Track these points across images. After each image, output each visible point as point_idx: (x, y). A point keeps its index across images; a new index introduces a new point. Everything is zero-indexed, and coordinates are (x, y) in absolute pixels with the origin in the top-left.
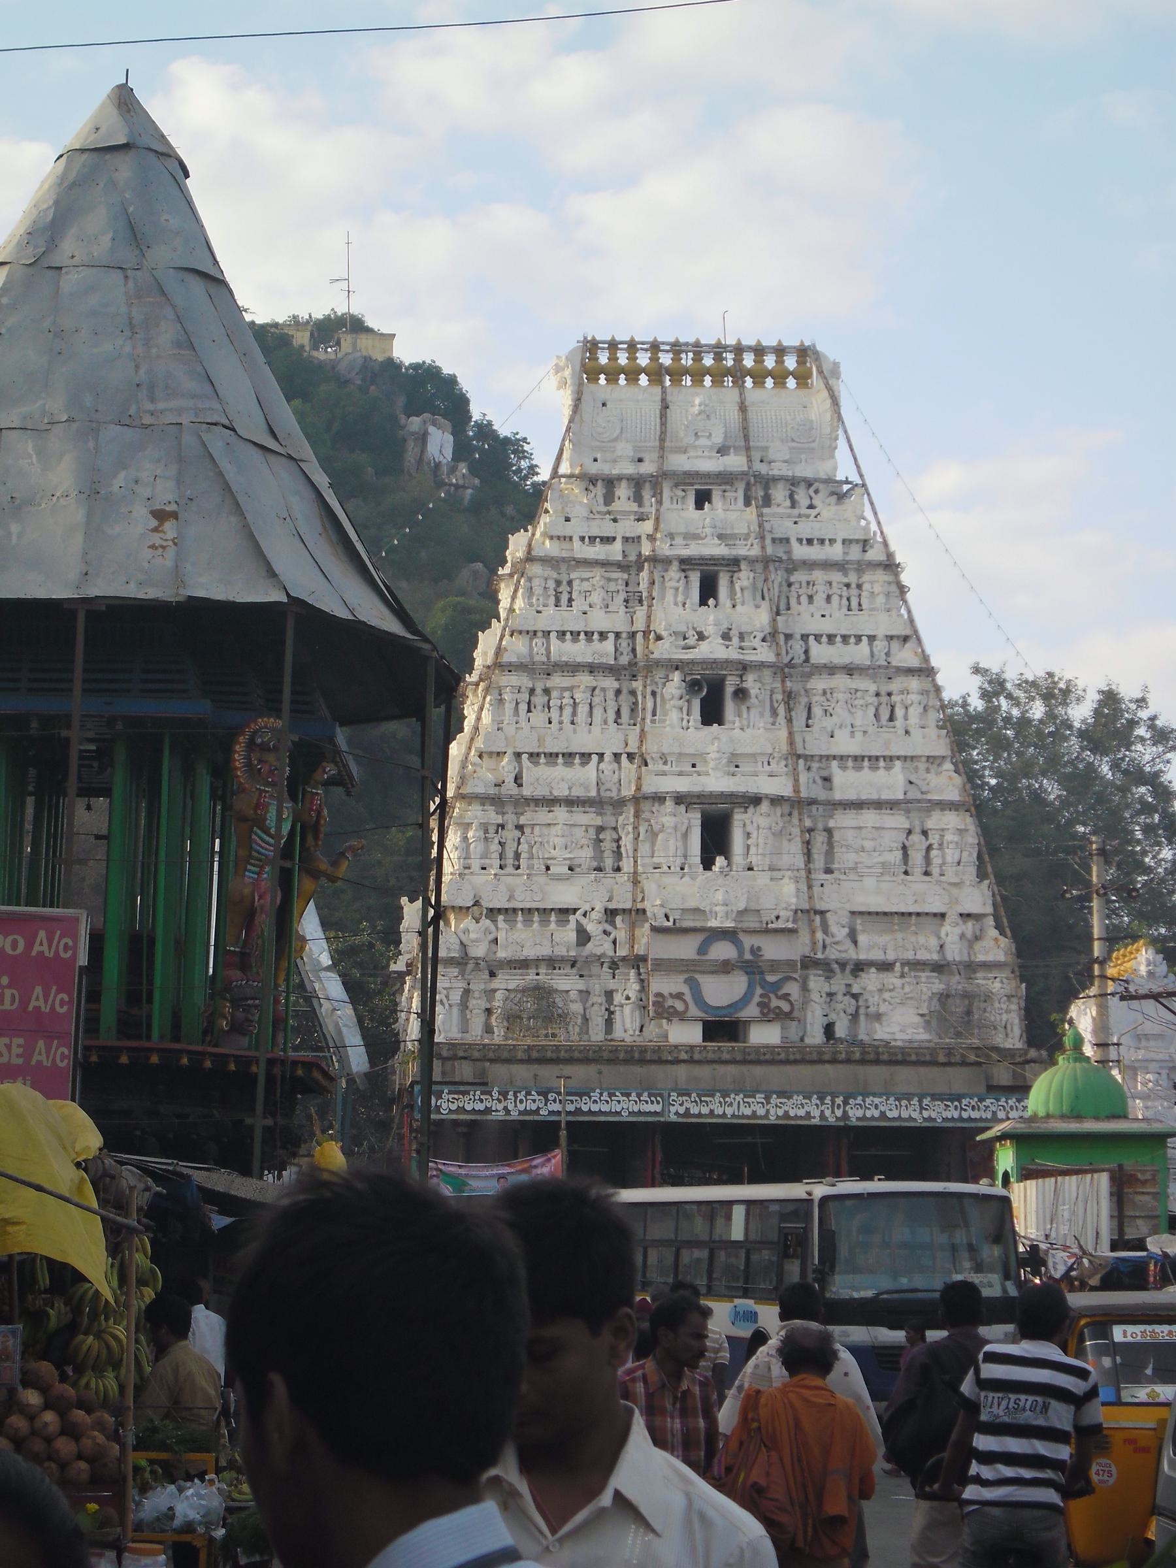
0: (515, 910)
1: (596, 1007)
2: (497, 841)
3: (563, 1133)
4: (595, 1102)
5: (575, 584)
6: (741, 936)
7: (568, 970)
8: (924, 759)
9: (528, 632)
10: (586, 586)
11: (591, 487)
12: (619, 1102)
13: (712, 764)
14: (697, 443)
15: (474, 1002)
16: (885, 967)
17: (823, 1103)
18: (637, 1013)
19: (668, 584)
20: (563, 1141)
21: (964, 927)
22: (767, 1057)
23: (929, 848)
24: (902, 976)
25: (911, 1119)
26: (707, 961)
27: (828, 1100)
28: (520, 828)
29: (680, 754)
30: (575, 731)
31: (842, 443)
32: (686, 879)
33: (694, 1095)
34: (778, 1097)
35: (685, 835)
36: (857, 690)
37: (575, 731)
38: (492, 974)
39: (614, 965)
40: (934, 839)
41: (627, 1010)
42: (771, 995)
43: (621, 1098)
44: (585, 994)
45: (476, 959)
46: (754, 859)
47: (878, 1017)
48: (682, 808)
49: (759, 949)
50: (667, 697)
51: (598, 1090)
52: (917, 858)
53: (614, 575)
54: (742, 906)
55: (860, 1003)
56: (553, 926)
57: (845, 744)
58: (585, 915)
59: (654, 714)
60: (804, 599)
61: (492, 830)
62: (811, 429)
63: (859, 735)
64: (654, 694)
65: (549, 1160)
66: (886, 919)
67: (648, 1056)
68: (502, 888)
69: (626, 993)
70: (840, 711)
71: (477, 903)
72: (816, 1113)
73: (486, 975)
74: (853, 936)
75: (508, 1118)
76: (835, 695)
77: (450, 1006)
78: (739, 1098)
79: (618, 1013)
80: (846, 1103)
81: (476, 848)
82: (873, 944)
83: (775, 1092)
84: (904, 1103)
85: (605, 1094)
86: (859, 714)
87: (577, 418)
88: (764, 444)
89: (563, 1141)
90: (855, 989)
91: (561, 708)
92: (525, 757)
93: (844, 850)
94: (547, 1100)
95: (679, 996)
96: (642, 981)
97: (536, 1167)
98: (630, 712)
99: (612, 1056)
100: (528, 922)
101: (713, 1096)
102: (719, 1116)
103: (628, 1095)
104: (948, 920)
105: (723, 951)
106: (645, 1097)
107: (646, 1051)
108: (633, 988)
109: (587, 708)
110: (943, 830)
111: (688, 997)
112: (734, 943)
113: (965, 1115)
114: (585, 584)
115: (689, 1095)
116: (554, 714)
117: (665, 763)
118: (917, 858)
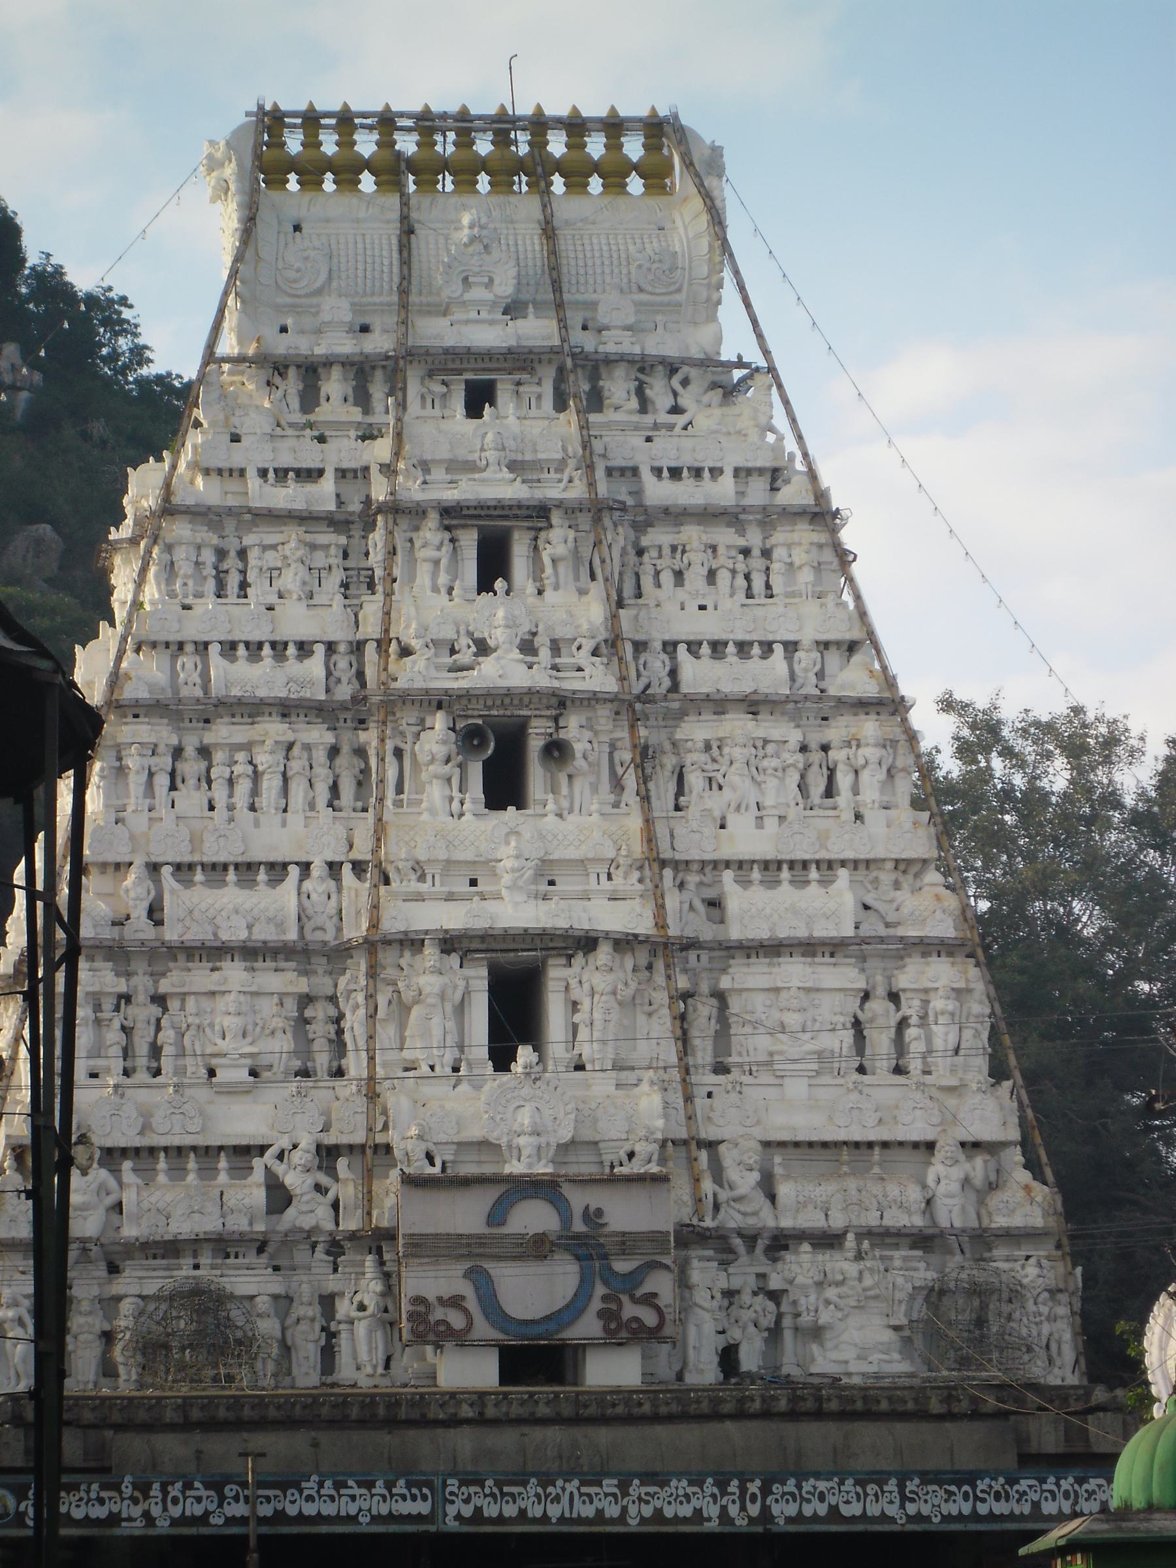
0: (152, 1151)
1: (303, 1327)
2: (116, 1024)
4: (310, 1498)
5: (253, 555)
6: (567, 1190)
7: (252, 1258)
8: (890, 865)
9: (167, 645)
11: (277, 380)
13: (506, 879)
14: (467, 296)
16: (827, 1240)
17: (724, 1493)
18: (379, 1334)
19: (421, 554)
22: (620, 1410)
23: (903, 1024)
24: (859, 1257)
25: (884, 1518)
27: (734, 1486)
28: (160, 1000)
29: (449, 862)
31: (729, 292)
33: (489, 1483)
35: (461, 1009)
37: (257, 824)
40: (911, 1007)
41: (361, 1328)
42: (625, 1299)
43: (357, 1491)
46: (586, 1050)
47: (817, 1333)
48: (454, 959)
49: (599, 1212)
50: (423, 758)
51: (315, 1478)
52: (881, 1042)
53: (322, 539)
55: (785, 1308)
56: (223, 1178)
57: (748, 840)
58: (280, 1156)
59: (400, 790)
60: (667, 578)
61: (108, 1004)
63: (771, 824)
64: (398, 753)
67: (403, 1413)
68: (129, 1110)
69: (357, 1298)
70: (738, 781)
75: (151, 1532)
76: (726, 750)
79: (344, 1335)
80: (766, 1491)
82: (804, 1200)
85: (328, 1483)
86: (771, 783)
90: (775, 1283)
91: (231, 782)
92: (166, 871)
93: (748, 1029)
94: (222, 1498)
95: (455, 1302)
96: (387, 1276)
98: (359, 786)
100: (178, 1173)
101: (524, 1484)
102: (535, 1521)
103: (370, 1485)
104: (939, 1154)
105: (533, 1217)
106: (400, 1488)
107: (398, 1403)
108: (371, 1288)
109: (277, 781)
111: (472, 1304)
113: (982, 1509)
114: (270, 554)
116: (219, 793)
117: (422, 878)
118: (881, 1042)
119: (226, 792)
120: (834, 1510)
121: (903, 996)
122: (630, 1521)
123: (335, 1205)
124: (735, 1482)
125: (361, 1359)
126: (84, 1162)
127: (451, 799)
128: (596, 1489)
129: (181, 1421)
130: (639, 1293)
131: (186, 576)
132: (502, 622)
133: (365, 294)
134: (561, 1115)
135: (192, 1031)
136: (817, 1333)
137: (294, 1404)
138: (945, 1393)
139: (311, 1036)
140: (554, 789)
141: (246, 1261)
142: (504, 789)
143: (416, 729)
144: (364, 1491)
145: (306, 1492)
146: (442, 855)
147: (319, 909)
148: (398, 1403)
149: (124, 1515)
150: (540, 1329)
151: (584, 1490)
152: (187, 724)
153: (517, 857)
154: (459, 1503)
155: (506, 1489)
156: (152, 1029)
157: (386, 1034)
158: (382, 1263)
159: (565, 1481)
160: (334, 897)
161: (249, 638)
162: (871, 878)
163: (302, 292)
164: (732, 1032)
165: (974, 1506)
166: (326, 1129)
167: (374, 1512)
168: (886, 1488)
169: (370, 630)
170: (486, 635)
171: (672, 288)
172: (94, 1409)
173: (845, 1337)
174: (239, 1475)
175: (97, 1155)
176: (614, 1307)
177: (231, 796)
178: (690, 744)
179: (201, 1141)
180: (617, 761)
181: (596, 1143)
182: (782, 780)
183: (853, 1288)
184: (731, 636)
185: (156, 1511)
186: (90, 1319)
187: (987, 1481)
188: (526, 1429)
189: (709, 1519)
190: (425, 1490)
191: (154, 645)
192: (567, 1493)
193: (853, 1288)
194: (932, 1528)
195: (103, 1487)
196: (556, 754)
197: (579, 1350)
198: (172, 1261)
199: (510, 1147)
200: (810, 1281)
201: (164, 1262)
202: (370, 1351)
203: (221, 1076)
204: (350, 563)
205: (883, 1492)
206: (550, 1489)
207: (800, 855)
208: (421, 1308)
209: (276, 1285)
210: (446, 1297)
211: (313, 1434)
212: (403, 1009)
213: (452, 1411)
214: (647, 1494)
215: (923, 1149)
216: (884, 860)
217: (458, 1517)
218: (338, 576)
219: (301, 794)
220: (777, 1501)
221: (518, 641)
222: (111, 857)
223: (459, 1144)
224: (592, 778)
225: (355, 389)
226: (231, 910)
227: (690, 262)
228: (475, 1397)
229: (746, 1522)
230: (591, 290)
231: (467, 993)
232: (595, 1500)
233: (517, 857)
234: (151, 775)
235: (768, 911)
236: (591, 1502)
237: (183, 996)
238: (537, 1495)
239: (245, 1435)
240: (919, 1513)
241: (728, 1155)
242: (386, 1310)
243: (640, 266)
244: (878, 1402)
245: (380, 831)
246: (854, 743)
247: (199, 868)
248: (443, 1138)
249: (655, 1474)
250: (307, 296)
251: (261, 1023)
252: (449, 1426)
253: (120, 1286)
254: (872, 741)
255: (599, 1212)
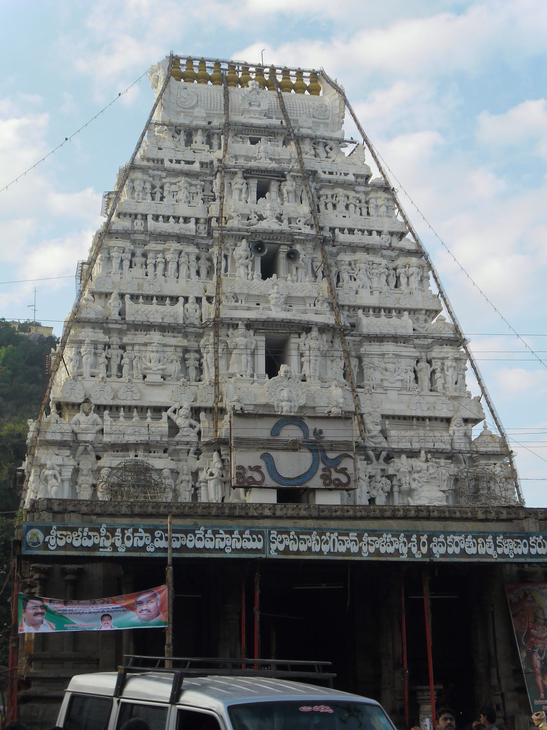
0: (118, 408)
1: (184, 484)
2: (104, 355)
3: (170, 570)
4: (200, 539)
5: (166, 188)
6: (307, 422)
7: (161, 454)
8: (424, 312)
9: (130, 215)
10: (174, 188)
11: (176, 135)
12: (222, 539)
13: (273, 302)
14: (251, 108)
15: (83, 478)
16: (413, 454)
17: (410, 541)
18: (219, 487)
19: (234, 187)
20: (169, 577)
21: (466, 428)
22: (339, 513)
23: (433, 372)
24: (427, 461)
25: (487, 555)
26: (278, 440)
27: (414, 538)
28: (123, 347)
29: (248, 295)
30: (166, 281)
31: (348, 117)
32: (255, 384)
33: (292, 533)
34: (369, 536)
35: (253, 354)
36: (373, 264)
37: (166, 281)
38: (98, 458)
39: (198, 453)
40: (437, 365)
41: (211, 484)
42: (332, 470)
43: (225, 536)
44: (175, 473)
45: (85, 442)
46: (307, 370)
47: (410, 492)
48: (251, 332)
49: (321, 432)
50: (236, 257)
51: (202, 528)
52: (425, 377)
53: (194, 182)
54: (302, 402)
55: (395, 482)
56: (149, 420)
57: (366, 299)
58: (175, 412)
59: (226, 270)
60: (330, 206)
61: (100, 346)
62: (326, 110)
63: (376, 294)
64: (226, 257)
65: (155, 596)
66: (406, 422)
67: (237, 512)
68: (108, 389)
69: (210, 470)
70: (362, 276)
71: (87, 401)
72: (404, 550)
73: (94, 458)
74: (384, 432)
75: (115, 554)
76: (358, 265)
77: (62, 481)
78: (334, 536)
79: (202, 488)
80: (430, 541)
81: (87, 359)
82: (400, 437)
83: (366, 531)
84: (480, 540)
85: (209, 531)
86: (375, 279)
87: (167, 90)
88: (295, 118)
89: (169, 577)
90: (391, 471)
91: (155, 266)
92: (127, 297)
93: (372, 370)
94: (153, 538)
95: (257, 469)
96: (223, 461)
97: (141, 603)
99: (205, 512)
100: (129, 417)
101: (310, 534)
102: (316, 553)
103: (231, 533)
104: (453, 423)
105: (291, 433)
106: (247, 535)
107: (235, 508)
108: (215, 464)
109: (175, 266)
110: (443, 359)
111: (264, 470)
112: (299, 425)
113: (533, 551)
114: (173, 186)
115: (288, 533)
116: (150, 269)
117: (237, 301)
118: (425, 377)
119: (153, 269)
120: (463, 551)
121: (433, 361)
122: (363, 554)
123: (199, 433)
124: (415, 536)
125: (211, 493)
126: (87, 411)
127: (248, 274)
128: (347, 538)
129: (130, 513)
130: (338, 468)
131: (139, 191)
132: (269, 208)
133: (210, 110)
134: (300, 394)
135: (137, 359)
136: (410, 492)
137: (185, 507)
138: (485, 510)
139: (188, 365)
140: (289, 271)
141: (159, 454)
142: (268, 270)
143: (233, 247)
144: (228, 536)
145: (198, 536)
146: (246, 291)
147: (191, 315)
148: (235, 508)
149: (101, 545)
150: (292, 483)
151: (340, 538)
152: (137, 245)
153: (278, 293)
154: (277, 543)
155: (301, 537)
156: (119, 359)
157: (222, 363)
158: (220, 456)
159: (331, 533)
160: (198, 311)
161: (165, 214)
162: (416, 317)
163: (186, 107)
164: (364, 372)
165: (529, 550)
166: (195, 400)
167: (233, 547)
168: (487, 540)
169: (214, 213)
170: (262, 213)
171: (325, 117)
172: (87, 506)
173: (422, 494)
174: (163, 526)
175: (93, 407)
176: (328, 473)
177: (155, 271)
178: (343, 262)
179: (139, 403)
180: (314, 266)
181: (314, 408)
182: (379, 278)
183: (425, 474)
184: (356, 227)
185: (118, 543)
186: (87, 478)
187: (534, 537)
188: (296, 521)
189: (403, 554)
190: (260, 536)
191: (125, 215)
192: (332, 539)
193: (425, 474)
194: (510, 560)
195: (91, 530)
196: (292, 256)
197: (314, 490)
198: (126, 453)
199: (278, 406)
200: (407, 470)
201: (122, 453)
202: (215, 494)
203: (149, 378)
204: (205, 193)
205: (486, 542)
206: (323, 537)
207: (388, 305)
208: (241, 471)
209: (172, 465)
210: (252, 467)
211: (194, 520)
212: (229, 352)
213: (260, 512)
214: (372, 541)
215: (445, 421)
216: (421, 310)
217: (277, 550)
218: (200, 196)
219: (185, 271)
220: (435, 546)
221: (275, 216)
222: (104, 290)
223: (255, 405)
224: (305, 270)
225: (207, 140)
226: (155, 313)
227: (332, 108)
228: (271, 506)
229: (420, 556)
230: (296, 115)
231: (256, 348)
232: (346, 543)
233: (278, 293)
234: (122, 261)
235: (378, 324)
236: (344, 545)
237: (133, 345)
238: (317, 540)
239: (161, 520)
240: (503, 553)
241: (368, 420)
242: (222, 476)
243: (314, 108)
244: (455, 513)
245: (219, 284)
246: (407, 266)
247: (141, 297)
248: (248, 402)
249: (375, 531)
250: (188, 108)
251: (167, 357)
252: (259, 519)
253: (101, 463)
254: (415, 265)
255: (321, 432)
